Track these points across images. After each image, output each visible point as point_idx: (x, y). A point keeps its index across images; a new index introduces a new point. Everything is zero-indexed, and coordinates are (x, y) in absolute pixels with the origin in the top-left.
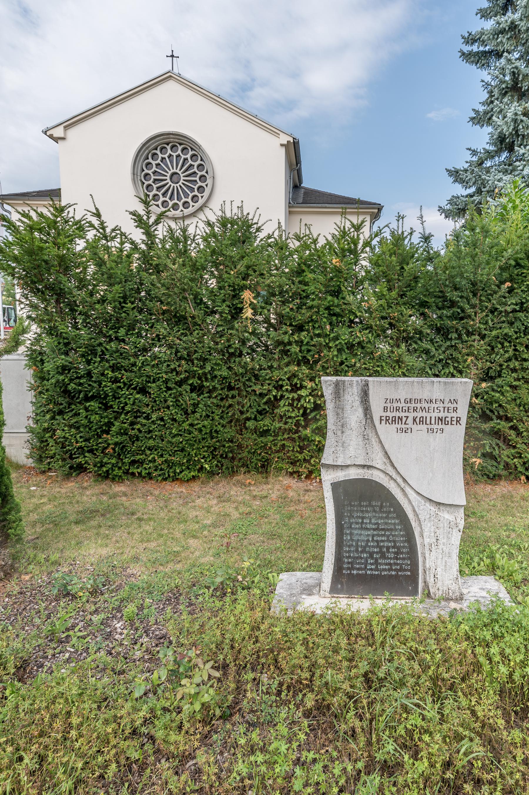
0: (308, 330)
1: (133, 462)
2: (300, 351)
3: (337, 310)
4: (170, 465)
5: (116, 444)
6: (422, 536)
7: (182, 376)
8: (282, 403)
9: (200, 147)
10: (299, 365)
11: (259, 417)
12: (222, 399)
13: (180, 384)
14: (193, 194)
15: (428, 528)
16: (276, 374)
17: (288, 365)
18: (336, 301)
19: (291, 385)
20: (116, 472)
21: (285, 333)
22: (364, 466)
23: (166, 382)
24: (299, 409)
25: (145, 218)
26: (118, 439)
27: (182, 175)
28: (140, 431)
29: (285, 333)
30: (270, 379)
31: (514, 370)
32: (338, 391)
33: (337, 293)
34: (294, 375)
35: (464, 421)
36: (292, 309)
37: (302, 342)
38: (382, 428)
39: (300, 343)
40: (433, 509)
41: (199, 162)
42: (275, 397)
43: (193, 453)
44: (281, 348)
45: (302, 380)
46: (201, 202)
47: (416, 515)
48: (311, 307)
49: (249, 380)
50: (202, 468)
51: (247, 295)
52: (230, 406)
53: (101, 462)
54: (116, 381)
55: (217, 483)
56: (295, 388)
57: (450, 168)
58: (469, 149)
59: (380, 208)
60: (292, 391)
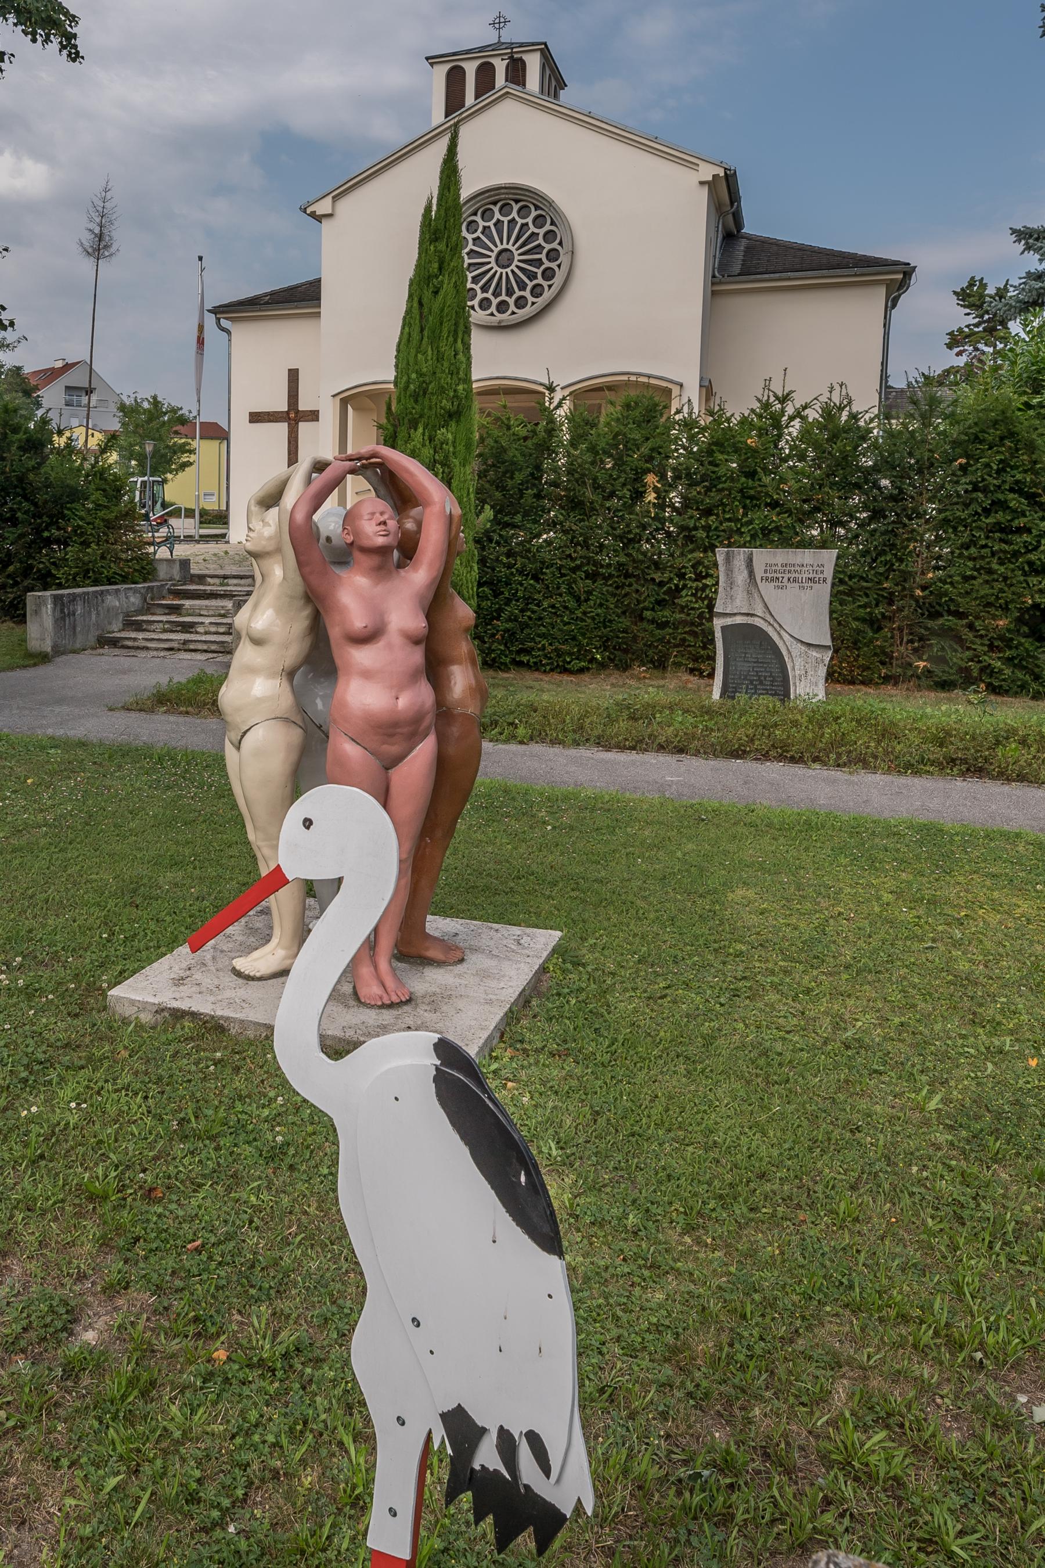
0: (717, 515)
1: (519, 652)
3: (752, 492)
4: (559, 654)
5: (506, 630)
6: (793, 669)
8: (684, 593)
9: (551, 204)
10: (705, 551)
12: (617, 588)
13: (574, 570)
14: (535, 282)
15: (799, 663)
16: (679, 562)
17: (692, 551)
18: (750, 482)
21: (691, 517)
22: (748, 615)
23: (559, 569)
24: (703, 600)
26: (509, 625)
27: (516, 253)
28: (530, 618)
29: (691, 517)
32: (728, 559)
33: (752, 475)
34: (699, 563)
35: (829, 581)
36: (699, 493)
37: (710, 527)
39: (707, 528)
41: (548, 227)
42: (677, 586)
46: (547, 295)
47: (789, 652)
48: (723, 489)
50: (593, 660)
51: (651, 479)
52: (626, 595)
53: (489, 648)
54: (509, 566)
56: (699, 577)
59: (908, 271)
60: (696, 580)
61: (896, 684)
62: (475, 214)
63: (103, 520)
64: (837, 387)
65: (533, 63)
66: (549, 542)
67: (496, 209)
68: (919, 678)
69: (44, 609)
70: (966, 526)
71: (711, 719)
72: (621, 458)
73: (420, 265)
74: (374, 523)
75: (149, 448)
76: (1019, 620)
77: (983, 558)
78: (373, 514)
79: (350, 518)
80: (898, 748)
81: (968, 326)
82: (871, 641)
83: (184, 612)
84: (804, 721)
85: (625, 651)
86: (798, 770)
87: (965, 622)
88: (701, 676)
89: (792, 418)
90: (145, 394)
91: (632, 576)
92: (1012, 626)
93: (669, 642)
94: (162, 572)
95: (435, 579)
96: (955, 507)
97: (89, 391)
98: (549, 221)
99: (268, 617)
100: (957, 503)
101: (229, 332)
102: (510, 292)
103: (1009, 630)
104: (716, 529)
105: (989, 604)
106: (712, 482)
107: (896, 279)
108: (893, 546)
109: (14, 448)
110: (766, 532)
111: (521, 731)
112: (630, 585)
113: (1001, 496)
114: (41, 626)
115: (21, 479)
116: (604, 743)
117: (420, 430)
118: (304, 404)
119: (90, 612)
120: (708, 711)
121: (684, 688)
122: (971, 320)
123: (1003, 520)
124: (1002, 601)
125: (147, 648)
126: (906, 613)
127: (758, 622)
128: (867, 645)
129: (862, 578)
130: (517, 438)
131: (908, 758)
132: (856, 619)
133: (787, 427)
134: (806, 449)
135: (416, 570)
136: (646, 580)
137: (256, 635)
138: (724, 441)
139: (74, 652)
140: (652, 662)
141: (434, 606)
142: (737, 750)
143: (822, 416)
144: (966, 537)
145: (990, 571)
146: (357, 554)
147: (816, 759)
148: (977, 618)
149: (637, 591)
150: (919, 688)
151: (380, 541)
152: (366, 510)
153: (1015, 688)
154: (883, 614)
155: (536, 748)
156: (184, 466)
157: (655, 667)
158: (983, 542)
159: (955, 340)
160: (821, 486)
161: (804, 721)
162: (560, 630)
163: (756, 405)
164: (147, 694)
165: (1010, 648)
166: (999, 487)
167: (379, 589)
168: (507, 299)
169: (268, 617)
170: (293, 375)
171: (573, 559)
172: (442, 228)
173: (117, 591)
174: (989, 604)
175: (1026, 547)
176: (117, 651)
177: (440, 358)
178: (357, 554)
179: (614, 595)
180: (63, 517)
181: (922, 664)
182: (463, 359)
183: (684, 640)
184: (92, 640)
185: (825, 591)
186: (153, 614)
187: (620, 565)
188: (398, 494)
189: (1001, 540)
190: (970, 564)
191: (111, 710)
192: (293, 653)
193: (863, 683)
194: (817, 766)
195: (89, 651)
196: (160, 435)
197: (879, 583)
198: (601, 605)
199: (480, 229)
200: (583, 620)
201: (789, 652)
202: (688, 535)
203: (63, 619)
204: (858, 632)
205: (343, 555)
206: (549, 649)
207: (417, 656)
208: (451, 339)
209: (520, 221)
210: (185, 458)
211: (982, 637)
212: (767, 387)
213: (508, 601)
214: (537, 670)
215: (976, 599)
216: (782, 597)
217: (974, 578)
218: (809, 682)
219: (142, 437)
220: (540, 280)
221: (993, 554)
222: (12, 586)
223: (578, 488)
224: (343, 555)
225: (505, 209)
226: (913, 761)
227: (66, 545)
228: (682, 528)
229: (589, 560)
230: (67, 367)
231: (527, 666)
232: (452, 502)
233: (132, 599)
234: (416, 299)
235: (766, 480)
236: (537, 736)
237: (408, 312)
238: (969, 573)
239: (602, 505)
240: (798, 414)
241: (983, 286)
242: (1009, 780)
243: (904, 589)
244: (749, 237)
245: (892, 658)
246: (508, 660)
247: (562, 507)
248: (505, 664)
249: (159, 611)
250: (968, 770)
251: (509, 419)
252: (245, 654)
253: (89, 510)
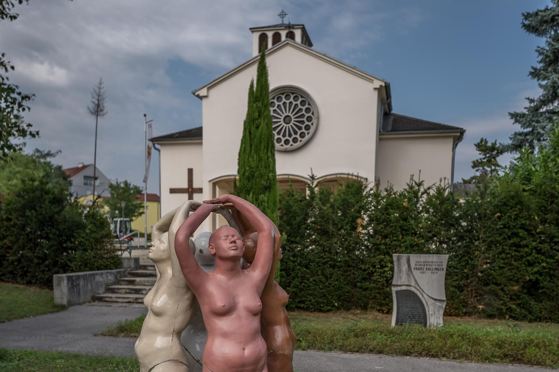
0: (390, 238)
1: (300, 302)
2: (386, 248)
3: (406, 228)
5: (293, 292)
6: (429, 311)
7: (326, 260)
8: (375, 274)
9: (308, 95)
10: (384, 255)
11: (363, 281)
12: (344, 272)
13: (324, 264)
14: (301, 131)
15: (431, 308)
16: (373, 260)
17: (379, 255)
18: (405, 223)
19: (380, 265)
20: (292, 306)
23: (318, 263)
24: (384, 277)
25: (311, 185)
26: (294, 290)
27: (293, 117)
28: (304, 286)
29: (378, 239)
30: (369, 262)
31: (503, 259)
32: (399, 259)
33: (405, 219)
36: (382, 228)
37: (387, 243)
38: (416, 273)
39: (385, 244)
40: (433, 301)
41: (307, 106)
42: (372, 271)
43: (330, 297)
44: (376, 246)
45: (386, 263)
46: (307, 137)
47: (427, 303)
48: (392, 226)
49: (359, 262)
50: (334, 306)
52: (349, 275)
54: (294, 262)
55: (341, 313)
56: (382, 267)
57: (512, 112)
58: (528, 99)
59: (462, 132)
60: (380, 268)
61: (469, 316)
62: (274, 98)
63: (94, 238)
64: (443, 179)
65: (298, 34)
66: (312, 250)
67: (283, 97)
68: (479, 313)
69: (62, 283)
70: (500, 244)
71: (393, 336)
72: (345, 211)
73: (249, 114)
74: (228, 241)
75: (123, 204)
76: (523, 287)
77: (508, 258)
78: (227, 236)
79: (213, 238)
80: (482, 349)
81: (480, 159)
82: (459, 296)
83: (136, 283)
84: (436, 337)
85: (349, 302)
86: (436, 361)
87: (500, 287)
88: (383, 313)
89: (423, 194)
90: (121, 180)
91: (351, 266)
92: (520, 289)
93: (368, 297)
94: (125, 264)
95: (266, 276)
96: (496, 235)
97: (96, 179)
98: (307, 103)
99: (163, 298)
100: (496, 234)
101: (159, 150)
102: (290, 135)
103: (519, 291)
104: (390, 244)
105: (510, 280)
106: (388, 222)
107: (457, 135)
108: (468, 253)
109: (47, 202)
110: (412, 246)
111: (303, 344)
112: (350, 271)
113: (516, 231)
114: (61, 290)
115: (51, 218)
116: (343, 349)
117: (251, 195)
118: (196, 185)
119: (87, 285)
120: (391, 332)
121: (376, 319)
122: (482, 156)
123: (516, 242)
124: (516, 278)
125: (117, 302)
126: (474, 283)
127: (413, 289)
128: (456, 298)
129: (454, 267)
130: (297, 201)
131: (486, 355)
132: (452, 286)
133: (421, 197)
134: (429, 208)
135: (254, 270)
136: (358, 268)
137: (156, 310)
138: (393, 204)
139: (79, 304)
140: (361, 306)
141: (265, 292)
142: (407, 352)
143: (436, 193)
144: (500, 249)
145: (511, 265)
146: (218, 261)
147: (444, 356)
148: (505, 286)
149: (353, 274)
150: (480, 318)
151: (232, 253)
152: (223, 234)
153: (521, 317)
154: (464, 284)
155: (311, 352)
156: (141, 214)
157: (362, 309)
158: (508, 251)
159: (475, 165)
160: (436, 225)
161: (436, 337)
162: (318, 292)
163: (407, 187)
164: (115, 326)
165: (519, 299)
166: (515, 226)
167: (232, 282)
168: (289, 138)
169: (163, 298)
170: (190, 171)
171: (324, 259)
172: (260, 96)
173: (102, 274)
174: (510, 280)
175: (526, 254)
176: (101, 304)
177: (260, 160)
178: (218, 261)
179: (343, 275)
180: (73, 237)
181: (481, 307)
182: (272, 161)
183: (375, 296)
184: (89, 298)
185: (442, 274)
186: (121, 285)
187: (346, 261)
188: (242, 224)
189: (515, 251)
190: (502, 261)
191: (95, 335)
192: (179, 321)
193: (455, 315)
194: (444, 359)
195: (87, 304)
196: (129, 200)
197: (462, 270)
198: (337, 280)
199: (276, 106)
200: (329, 287)
201: (427, 303)
202: (377, 247)
203: (73, 288)
204: (453, 292)
205: (211, 260)
206: (313, 301)
207: (255, 323)
208: (265, 151)
209: (294, 103)
210: (141, 211)
211: (507, 294)
212: (412, 179)
213: (294, 278)
214: (308, 311)
215: (505, 277)
216: (422, 277)
217: (503, 268)
218: (435, 319)
219: (121, 200)
220: (303, 130)
221: (512, 257)
222: (48, 271)
223: (326, 225)
224: (211, 260)
225: (288, 97)
226: (489, 356)
227: (75, 251)
228: (374, 244)
229: (332, 259)
230: (84, 167)
231: (303, 309)
232: (275, 230)
233: (110, 278)
234: (248, 131)
235: (412, 222)
236: (311, 346)
237: (244, 137)
238: (502, 265)
239: (337, 233)
240: (425, 192)
241: (486, 142)
242: (533, 365)
243: (473, 272)
244: (394, 115)
245: (467, 304)
246: (294, 306)
247: (318, 234)
248: (292, 308)
249: (123, 283)
250: (514, 360)
251: (293, 192)
252: (151, 321)
253: (87, 234)
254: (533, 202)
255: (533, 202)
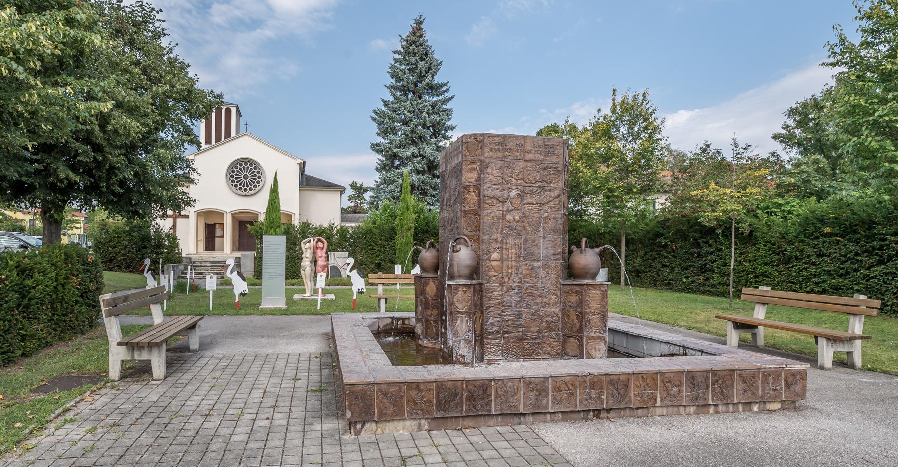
40: (630, 352)
254: (377, 232)
255: (377, 232)
